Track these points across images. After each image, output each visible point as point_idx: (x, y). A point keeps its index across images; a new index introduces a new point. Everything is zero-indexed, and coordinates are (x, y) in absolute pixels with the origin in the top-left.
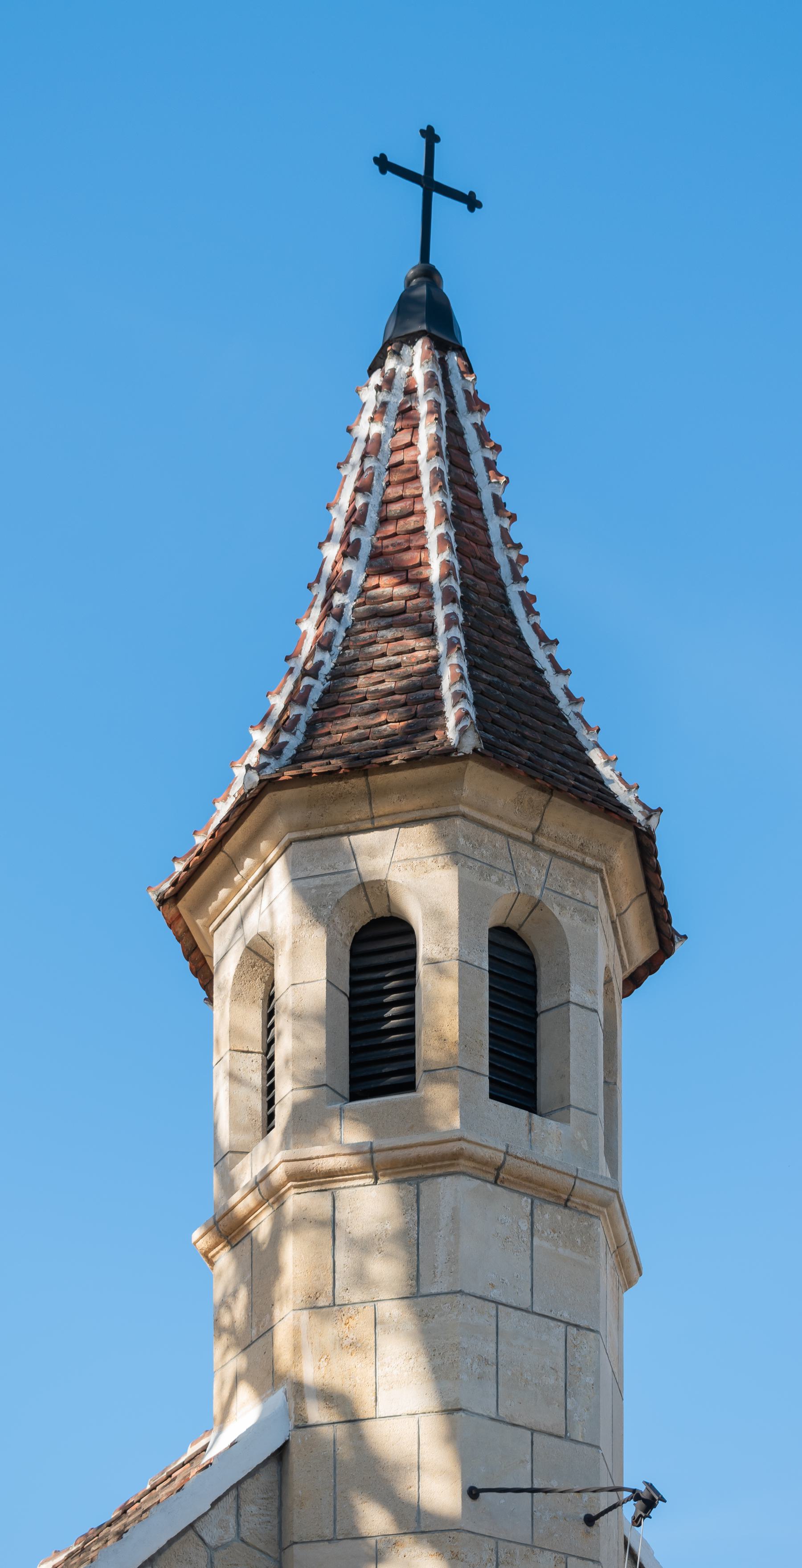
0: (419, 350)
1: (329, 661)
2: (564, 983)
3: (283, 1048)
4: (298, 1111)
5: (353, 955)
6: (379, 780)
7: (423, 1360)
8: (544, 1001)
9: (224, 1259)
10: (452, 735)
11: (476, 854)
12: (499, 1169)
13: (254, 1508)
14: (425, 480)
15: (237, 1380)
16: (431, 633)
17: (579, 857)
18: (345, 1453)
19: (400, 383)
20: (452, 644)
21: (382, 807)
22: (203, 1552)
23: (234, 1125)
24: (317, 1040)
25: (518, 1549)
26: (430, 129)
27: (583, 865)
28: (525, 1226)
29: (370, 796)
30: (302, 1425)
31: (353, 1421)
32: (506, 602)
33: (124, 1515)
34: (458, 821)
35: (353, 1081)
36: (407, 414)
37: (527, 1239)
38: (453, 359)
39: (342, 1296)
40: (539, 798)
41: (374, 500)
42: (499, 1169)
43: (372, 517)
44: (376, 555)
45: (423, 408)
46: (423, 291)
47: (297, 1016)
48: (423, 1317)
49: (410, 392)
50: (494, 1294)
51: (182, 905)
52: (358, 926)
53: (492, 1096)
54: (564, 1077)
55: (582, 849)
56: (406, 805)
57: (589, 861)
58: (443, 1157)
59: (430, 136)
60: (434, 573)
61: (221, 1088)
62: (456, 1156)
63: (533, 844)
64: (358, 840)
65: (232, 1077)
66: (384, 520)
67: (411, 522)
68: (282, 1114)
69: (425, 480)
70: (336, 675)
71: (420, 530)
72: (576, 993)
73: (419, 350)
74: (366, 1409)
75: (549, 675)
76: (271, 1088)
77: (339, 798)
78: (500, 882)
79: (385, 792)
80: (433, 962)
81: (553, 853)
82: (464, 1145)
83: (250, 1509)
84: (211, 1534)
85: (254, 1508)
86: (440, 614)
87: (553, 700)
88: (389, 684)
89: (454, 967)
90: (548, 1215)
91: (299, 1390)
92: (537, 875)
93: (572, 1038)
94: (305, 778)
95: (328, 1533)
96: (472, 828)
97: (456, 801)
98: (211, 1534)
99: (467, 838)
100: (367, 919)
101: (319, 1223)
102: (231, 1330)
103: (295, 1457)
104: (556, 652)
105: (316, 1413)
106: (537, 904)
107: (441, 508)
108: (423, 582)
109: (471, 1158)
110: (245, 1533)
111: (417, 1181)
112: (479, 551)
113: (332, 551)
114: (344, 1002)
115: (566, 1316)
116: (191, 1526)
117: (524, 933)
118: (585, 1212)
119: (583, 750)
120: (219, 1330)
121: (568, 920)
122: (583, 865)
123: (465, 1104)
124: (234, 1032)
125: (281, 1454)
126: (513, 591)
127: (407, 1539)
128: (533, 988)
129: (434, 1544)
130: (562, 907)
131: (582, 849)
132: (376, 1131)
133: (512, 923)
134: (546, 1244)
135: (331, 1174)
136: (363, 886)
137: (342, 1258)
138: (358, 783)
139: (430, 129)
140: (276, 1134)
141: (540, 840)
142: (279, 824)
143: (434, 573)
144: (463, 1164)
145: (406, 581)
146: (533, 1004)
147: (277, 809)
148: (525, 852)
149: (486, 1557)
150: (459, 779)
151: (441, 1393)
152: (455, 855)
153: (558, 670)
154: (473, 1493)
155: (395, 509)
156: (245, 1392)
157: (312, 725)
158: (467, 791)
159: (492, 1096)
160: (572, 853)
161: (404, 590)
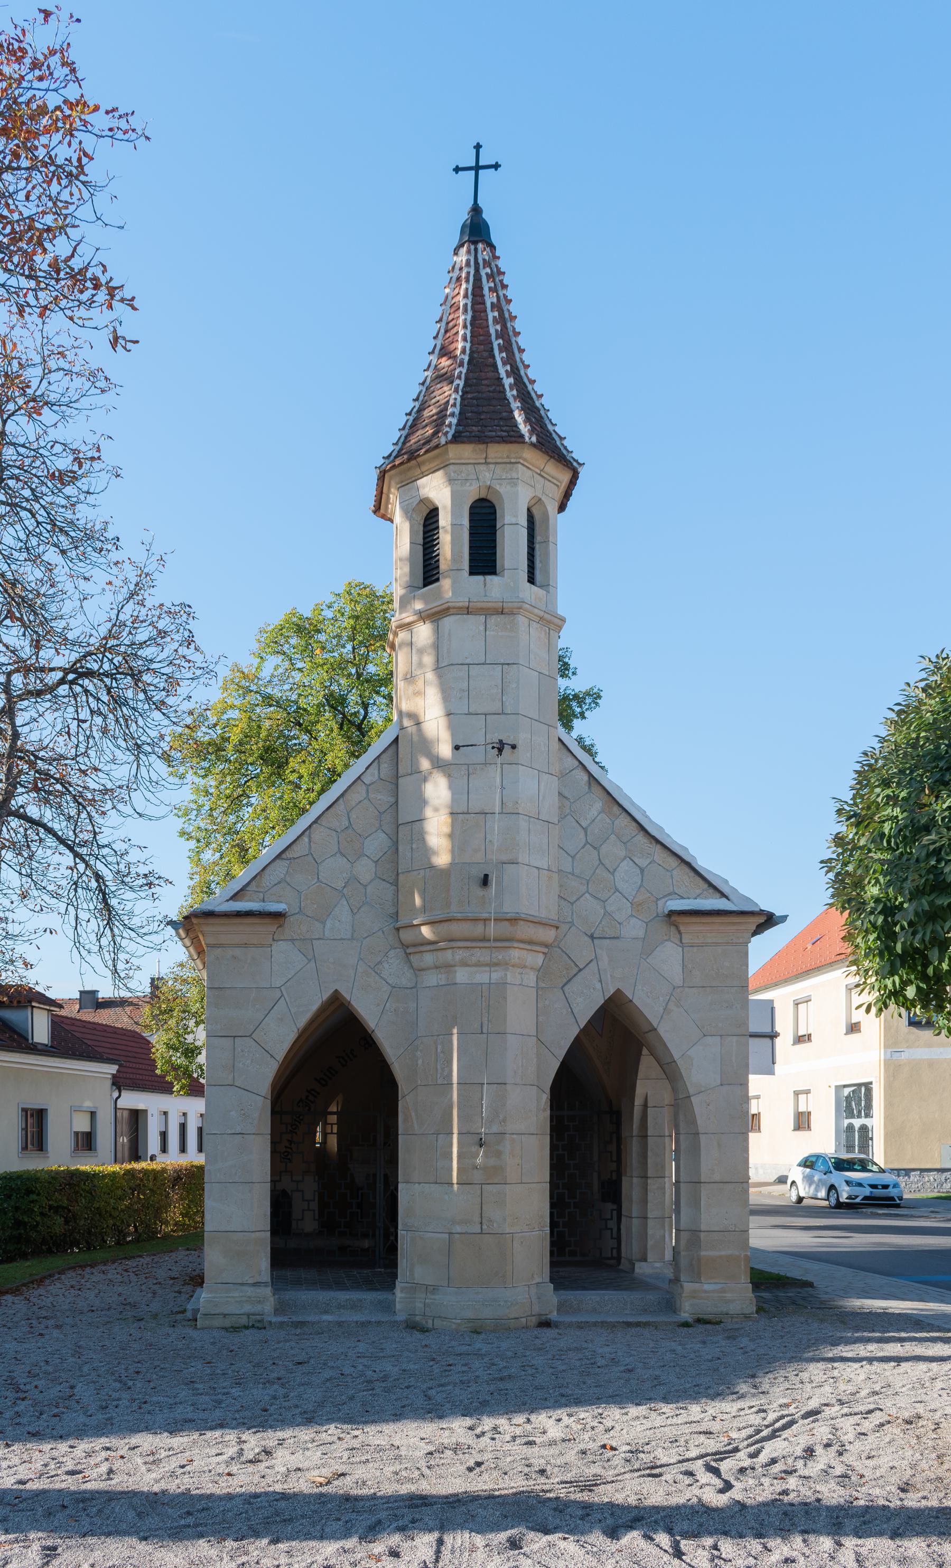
2: (503, 516)
6: (419, 459)
7: (440, 695)
11: (459, 477)
12: (468, 608)
13: (386, 765)
17: (508, 460)
18: (415, 738)
21: (424, 468)
22: (364, 787)
25: (478, 767)
26: (454, 170)
27: (511, 463)
28: (482, 628)
29: (419, 465)
31: (418, 724)
33: (392, 910)
34: (451, 467)
35: (425, 579)
37: (483, 633)
40: (482, 447)
42: (468, 608)
48: (440, 676)
50: (468, 661)
51: (382, 511)
52: (425, 514)
55: (508, 457)
56: (432, 465)
57: (513, 460)
58: (444, 610)
62: (448, 609)
63: (486, 463)
74: (422, 719)
77: (409, 469)
78: (471, 484)
79: (424, 463)
80: (443, 528)
81: (496, 463)
82: (450, 604)
85: (386, 765)
90: (493, 620)
93: (506, 539)
94: (394, 467)
95: (409, 772)
96: (457, 467)
97: (449, 459)
99: (454, 472)
100: (428, 511)
105: (406, 723)
106: (489, 487)
109: (454, 608)
110: (382, 776)
112: (481, 331)
114: (421, 548)
115: (502, 661)
116: (359, 778)
117: (489, 498)
121: (503, 489)
122: (511, 463)
125: (396, 740)
127: (435, 771)
129: (443, 771)
130: (500, 484)
131: (508, 457)
132: (426, 603)
133: (483, 496)
134: (492, 633)
135: (409, 624)
136: (422, 501)
137: (415, 658)
138: (413, 462)
139: (454, 170)
141: (488, 460)
142: (393, 483)
144: (452, 611)
145: (450, 358)
146: (495, 526)
147: (391, 478)
148: (483, 467)
149: (463, 773)
150: (447, 450)
151: (446, 707)
154: (457, 748)
155: (451, 324)
158: (451, 455)
160: (505, 460)
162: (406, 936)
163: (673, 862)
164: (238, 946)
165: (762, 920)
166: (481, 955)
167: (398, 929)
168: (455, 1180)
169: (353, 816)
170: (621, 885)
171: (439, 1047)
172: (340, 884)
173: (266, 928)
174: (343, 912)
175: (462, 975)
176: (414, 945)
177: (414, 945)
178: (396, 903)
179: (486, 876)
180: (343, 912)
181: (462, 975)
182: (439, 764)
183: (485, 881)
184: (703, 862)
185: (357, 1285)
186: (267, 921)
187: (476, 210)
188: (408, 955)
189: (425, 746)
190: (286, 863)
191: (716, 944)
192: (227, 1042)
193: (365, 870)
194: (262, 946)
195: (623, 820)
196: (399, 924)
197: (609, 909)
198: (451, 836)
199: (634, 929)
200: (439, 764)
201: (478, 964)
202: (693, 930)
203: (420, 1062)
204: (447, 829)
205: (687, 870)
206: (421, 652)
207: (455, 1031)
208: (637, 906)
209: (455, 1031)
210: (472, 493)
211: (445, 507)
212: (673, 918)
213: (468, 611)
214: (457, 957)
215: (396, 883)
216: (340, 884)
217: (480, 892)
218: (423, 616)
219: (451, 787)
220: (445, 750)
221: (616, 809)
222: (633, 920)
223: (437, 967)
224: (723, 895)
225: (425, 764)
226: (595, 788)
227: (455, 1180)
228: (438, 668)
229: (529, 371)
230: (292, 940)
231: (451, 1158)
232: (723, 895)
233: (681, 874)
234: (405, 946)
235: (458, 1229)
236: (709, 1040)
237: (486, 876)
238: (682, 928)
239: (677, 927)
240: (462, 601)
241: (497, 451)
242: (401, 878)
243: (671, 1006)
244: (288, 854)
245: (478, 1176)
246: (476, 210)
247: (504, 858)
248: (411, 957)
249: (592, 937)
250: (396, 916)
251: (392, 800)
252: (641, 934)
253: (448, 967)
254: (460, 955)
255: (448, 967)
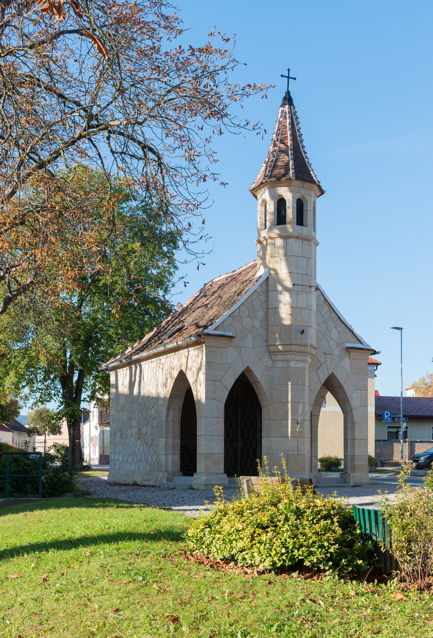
0: (287, 106)
1: (274, 159)
2: (307, 207)
3: (268, 217)
4: (270, 227)
5: (278, 203)
8: (304, 209)
9: (259, 245)
10: (291, 176)
14: (288, 128)
15: (261, 264)
16: (288, 155)
19: (284, 112)
20: (291, 159)
23: (260, 225)
24: (272, 217)
29: (280, 183)
30: (270, 274)
31: (277, 274)
32: (299, 146)
33: (266, 339)
36: (285, 117)
38: (292, 107)
39: (276, 255)
41: (281, 131)
43: (280, 134)
44: (281, 140)
45: (288, 116)
46: (287, 96)
47: (270, 213)
49: (286, 113)
53: (297, 224)
54: (307, 221)
59: (289, 70)
60: (289, 145)
61: (259, 219)
64: (278, 188)
65: (260, 218)
66: (282, 134)
67: (286, 135)
68: (267, 227)
69: (288, 128)
70: (275, 162)
71: (287, 137)
72: (309, 208)
73: (287, 106)
74: (279, 272)
75: (305, 159)
76: (266, 224)
80: (288, 207)
83: (263, 286)
84: (258, 291)
86: (290, 152)
87: (306, 163)
88: (283, 164)
89: (291, 208)
90: (305, 242)
91: (270, 269)
92: (303, 192)
98: (258, 291)
101: (273, 244)
102: (260, 256)
103: (269, 278)
104: (307, 155)
105: (272, 272)
107: (290, 134)
108: (287, 146)
111: (286, 239)
113: (274, 135)
118: (310, 241)
119: (310, 171)
120: (258, 256)
121: (307, 198)
123: (293, 228)
124: (260, 211)
125: (267, 278)
126: (300, 145)
128: (303, 207)
140: (267, 230)
143: (289, 145)
148: (302, 189)
152: (291, 191)
153: (307, 158)
154: (294, 285)
156: (262, 267)
157: (272, 171)
159: (297, 224)
161: (285, 147)
162: (272, 349)
163: (347, 330)
164: (216, 347)
165: (373, 352)
166: (299, 357)
167: (268, 346)
168: (290, 435)
169: (253, 304)
170: (333, 337)
171: (283, 389)
172: (249, 328)
173: (225, 341)
174: (250, 338)
175: (292, 364)
176: (274, 352)
177: (274, 352)
178: (267, 336)
179: (303, 331)
180: (250, 338)
181: (292, 364)
182: (286, 289)
183: (303, 332)
184: (356, 331)
185: (58, 506)
186: (228, 339)
187: (288, 93)
188: (270, 355)
189: (280, 282)
190: (232, 318)
191: (359, 359)
192: (212, 383)
193: (257, 323)
194: (224, 348)
195: (334, 315)
196: (269, 344)
197: (330, 344)
198: (291, 315)
199: (337, 352)
200: (286, 289)
201: (298, 361)
202: (354, 354)
203: (274, 394)
204: (289, 312)
205: (351, 333)
206: (279, 248)
207: (290, 383)
208: (338, 344)
209: (290, 383)
210: (298, 196)
211: (288, 200)
212: (348, 349)
213: (297, 238)
214: (292, 358)
215: (267, 329)
216: (249, 328)
217: (300, 335)
218: (280, 236)
219: (291, 298)
220: (289, 284)
221: (332, 310)
222: (337, 349)
223: (282, 360)
224: (361, 343)
225: (280, 288)
226: (326, 303)
227: (290, 435)
228: (286, 255)
229: (307, 155)
230: (234, 347)
231: (288, 428)
232: (361, 343)
233: (350, 334)
234: (270, 352)
235: (291, 453)
236: (357, 391)
237: (303, 331)
238: (351, 353)
239: (349, 353)
240: (296, 234)
241: (307, 185)
242: (270, 327)
243: (347, 379)
244: (233, 315)
245: (297, 435)
246: (288, 93)
247: (308, 324)
248: (272, 356)
249: (325, 354)
250: (267, 341)
251: (266, 299)
252: (339, 354)
253: (287, 361)
254: (293, 357)
255: (287, 361)
